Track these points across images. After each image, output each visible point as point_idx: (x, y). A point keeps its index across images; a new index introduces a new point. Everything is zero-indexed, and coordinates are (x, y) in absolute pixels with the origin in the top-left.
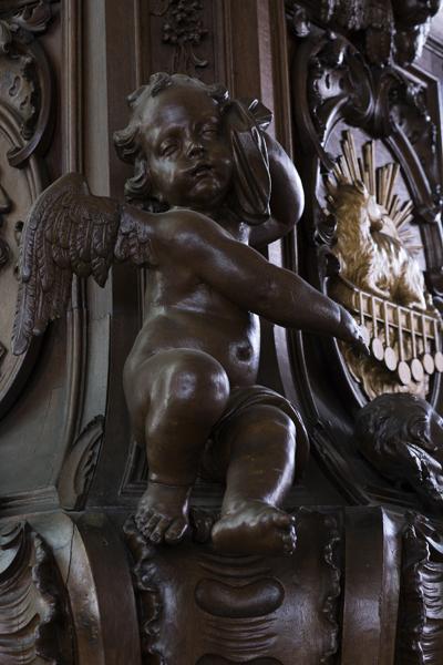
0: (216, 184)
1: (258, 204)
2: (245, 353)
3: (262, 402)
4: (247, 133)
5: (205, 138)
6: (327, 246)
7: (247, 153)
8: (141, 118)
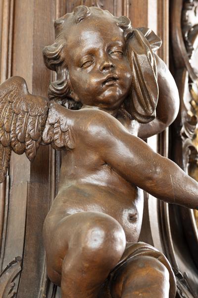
0: (119, 92)
1: (148, 108)
2: (132, 218)
3: (144, 255)
4: (144, 55)
5: (113, 56)
6: (189, 140)
7: (143, 70)
8: (66, 39)
